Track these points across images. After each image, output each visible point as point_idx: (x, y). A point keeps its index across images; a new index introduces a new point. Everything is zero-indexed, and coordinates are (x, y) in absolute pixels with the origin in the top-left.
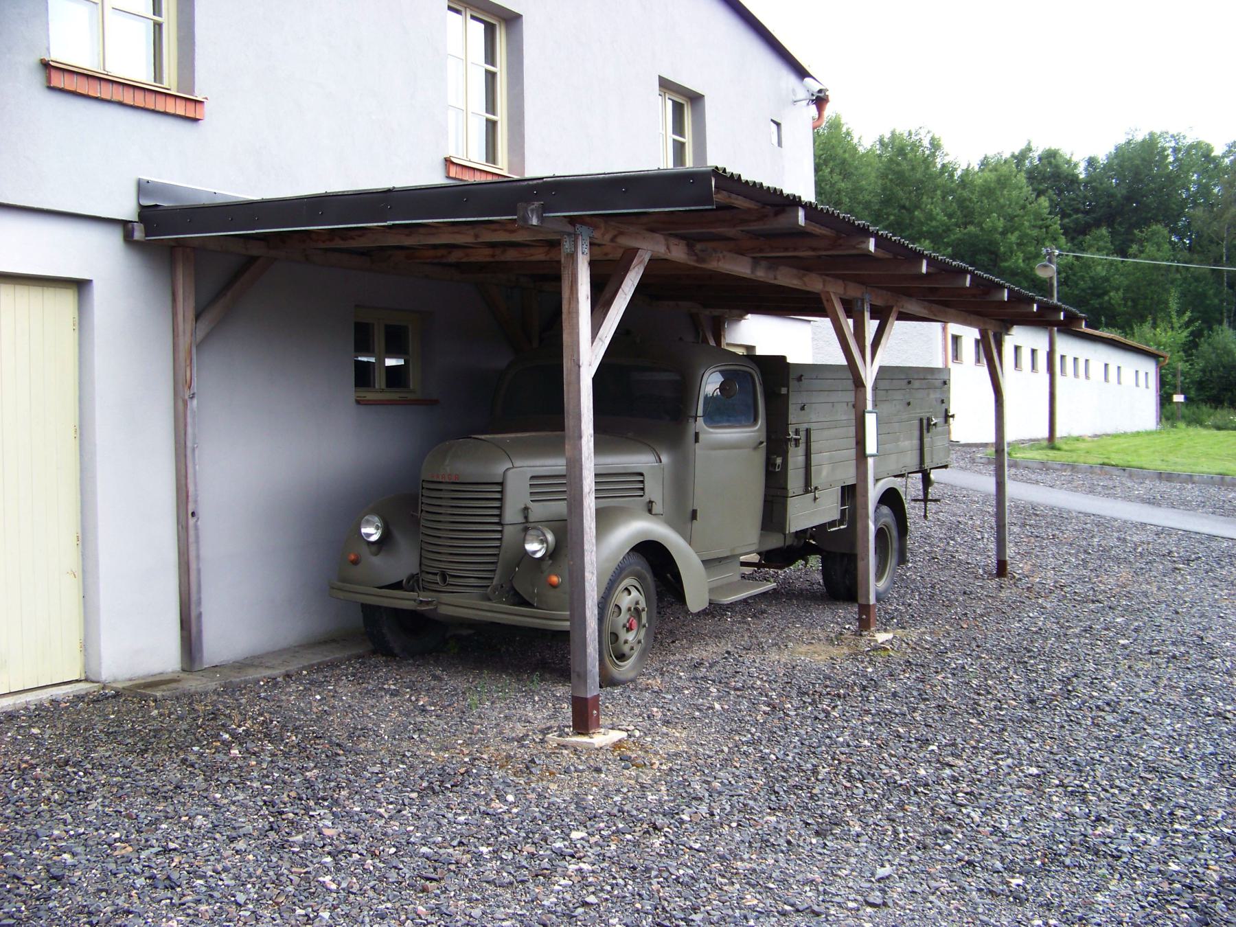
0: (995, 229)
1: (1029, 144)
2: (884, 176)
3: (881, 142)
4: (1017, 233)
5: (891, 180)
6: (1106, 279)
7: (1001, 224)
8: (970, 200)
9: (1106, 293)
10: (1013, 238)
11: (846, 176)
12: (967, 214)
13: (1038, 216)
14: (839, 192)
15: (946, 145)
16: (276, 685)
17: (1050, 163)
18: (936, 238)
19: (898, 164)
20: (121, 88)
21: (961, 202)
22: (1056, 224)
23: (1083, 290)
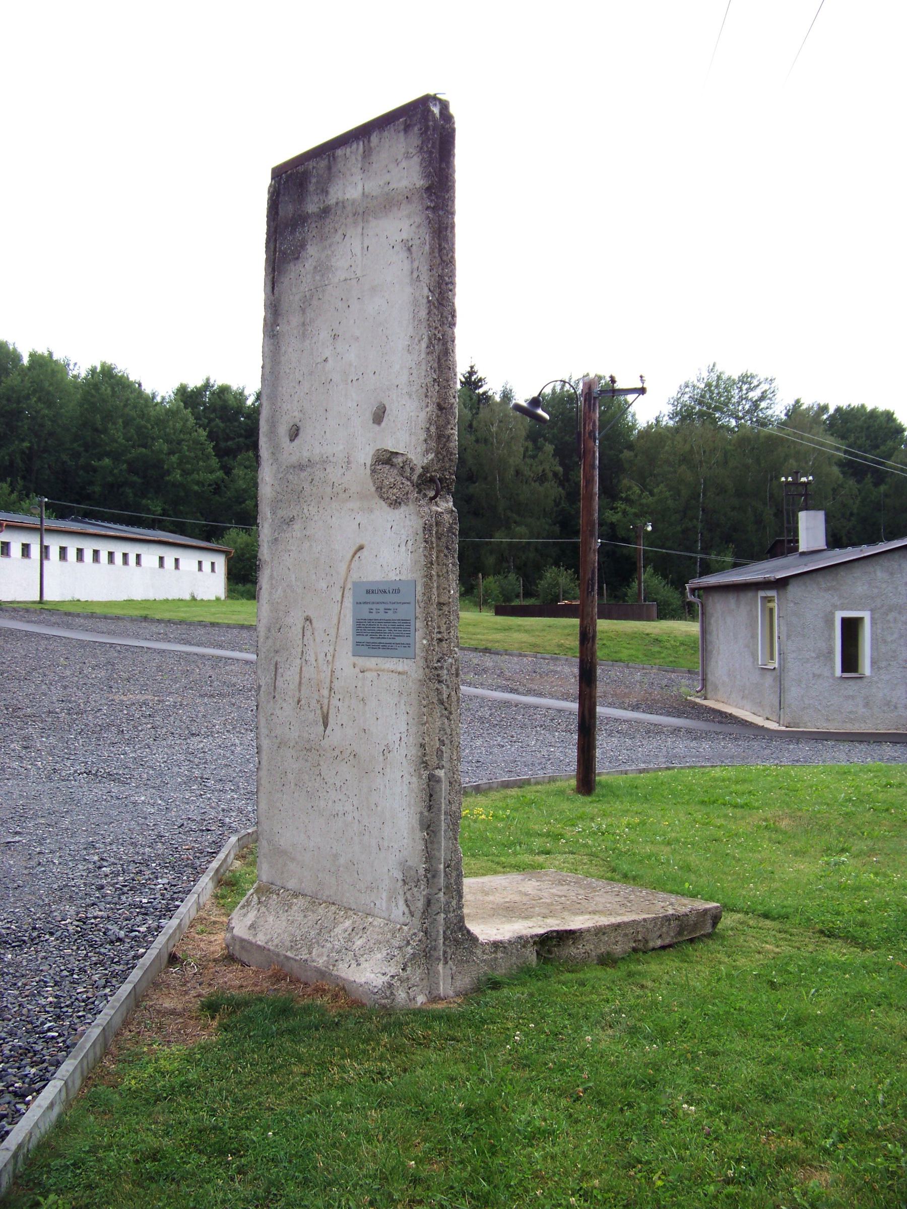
0: (161, 451)
1: (208, 380)
2: (81, 405)
3: (589, 386)
4: (177, 456)
5: (86, 409)
6: (245, 491)
7: (165, 447)
8: (146, 428)
9: (244, 502)
10: (174, 458)
11: (50, 404)
12: (144, 439)
13: (197, 442)
14: (43, 417)
15: (866, 405)
16: (149, 1103)
17: (220, 397)
18: (116, 456)
19: (93, 396)
20: (845, 747)
21: (139, 428)
22: (210, 448)
23: (229, 498)
